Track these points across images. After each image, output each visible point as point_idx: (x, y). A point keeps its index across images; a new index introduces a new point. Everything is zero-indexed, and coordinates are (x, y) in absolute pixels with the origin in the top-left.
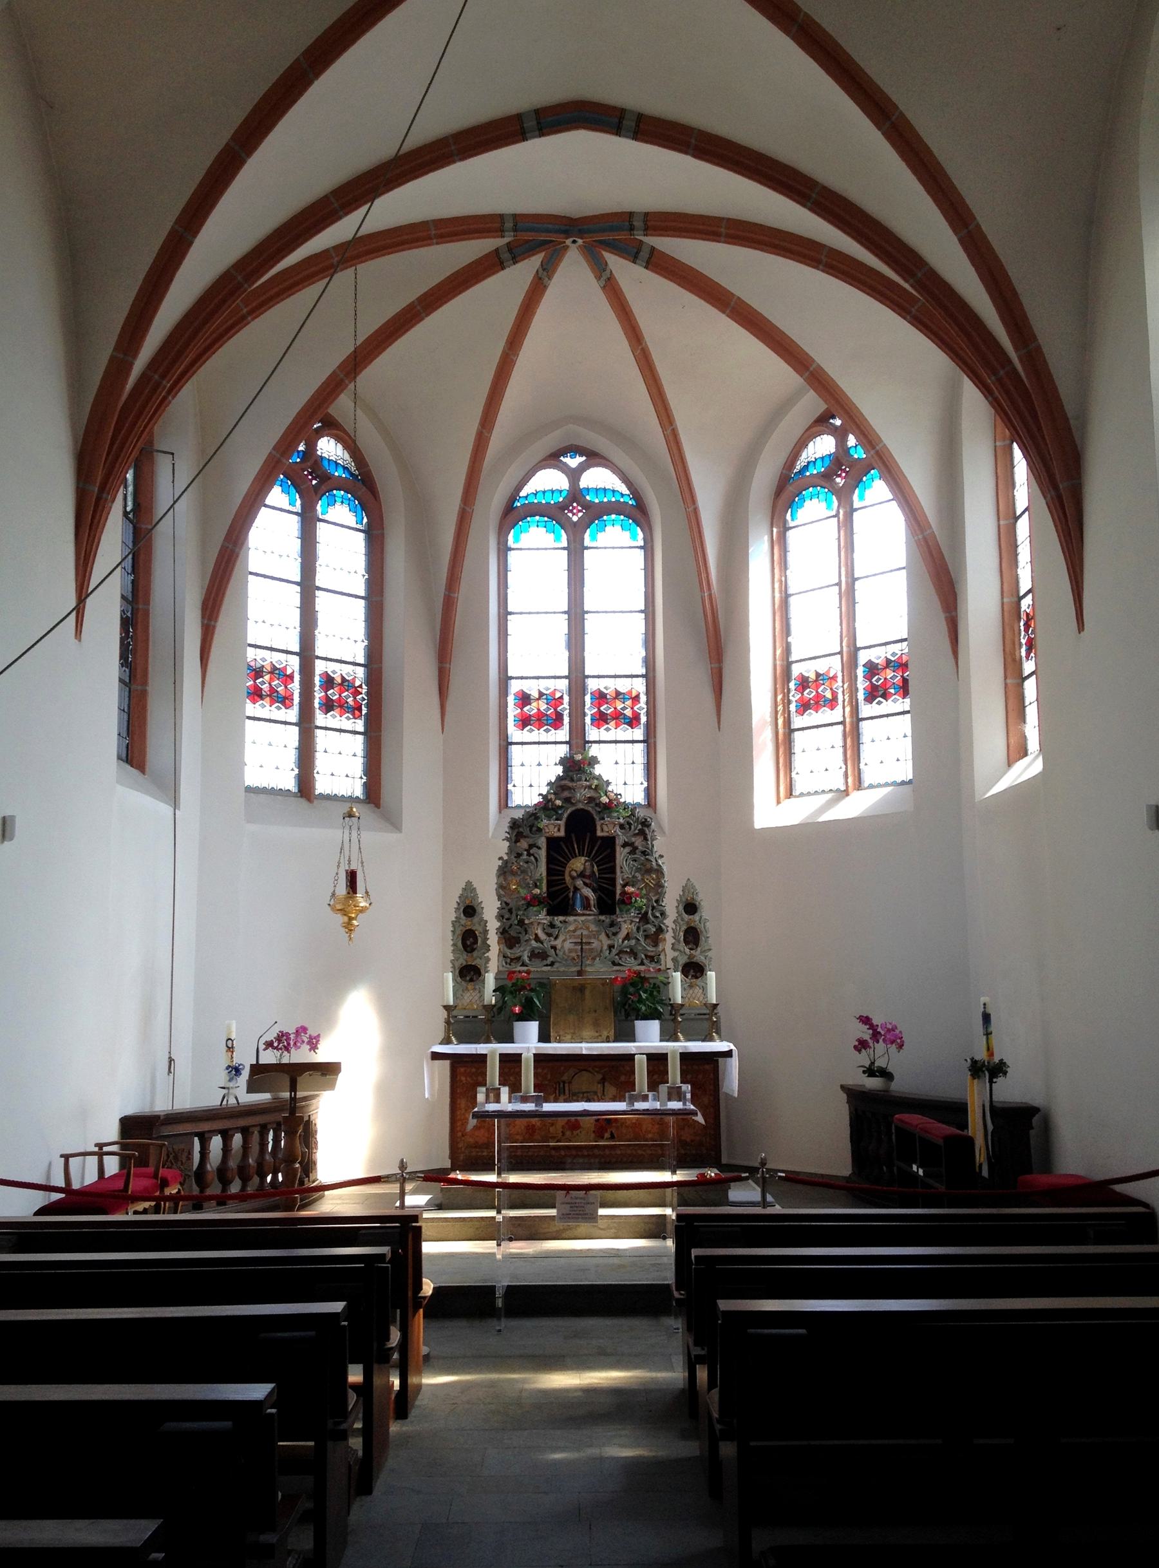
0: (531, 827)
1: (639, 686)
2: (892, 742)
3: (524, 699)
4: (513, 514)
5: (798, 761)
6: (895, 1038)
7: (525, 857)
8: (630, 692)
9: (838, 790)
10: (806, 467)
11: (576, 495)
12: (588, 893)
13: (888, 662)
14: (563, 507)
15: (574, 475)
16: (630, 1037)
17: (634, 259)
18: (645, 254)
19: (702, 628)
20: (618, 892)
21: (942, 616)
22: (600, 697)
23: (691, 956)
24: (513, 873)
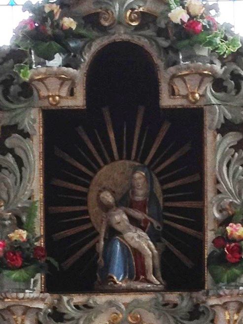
12: (140, 240)
20: (210, 236)
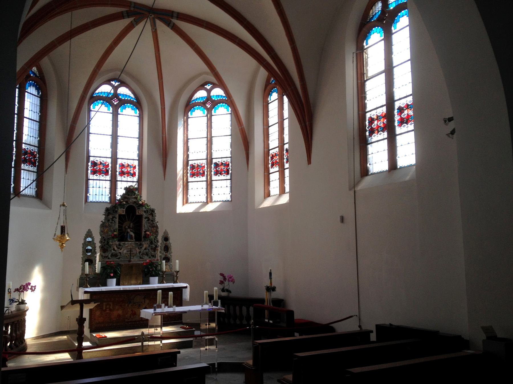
0: (113, 211)
1: (136, 163)
2: (222, 189)
3: (94, 164)
4: (94, 99)
5: (190, 192)
6: (231, 280)
7: (111, 221)
8: (133, 165)
9: (204, 202)
10: (197, 99)
11: (116, 95)
12: (132, 234)
13: (222, 163)
14: (112, 98)
15: (116, 88)
16: (148, 283)
17: (168, 25)
18: (172, 25)
19: (160, 145)
20: (143, 233)
21: (244, 152)
22: (122, 166)
23: (166, 255)
24: (106, 227)
